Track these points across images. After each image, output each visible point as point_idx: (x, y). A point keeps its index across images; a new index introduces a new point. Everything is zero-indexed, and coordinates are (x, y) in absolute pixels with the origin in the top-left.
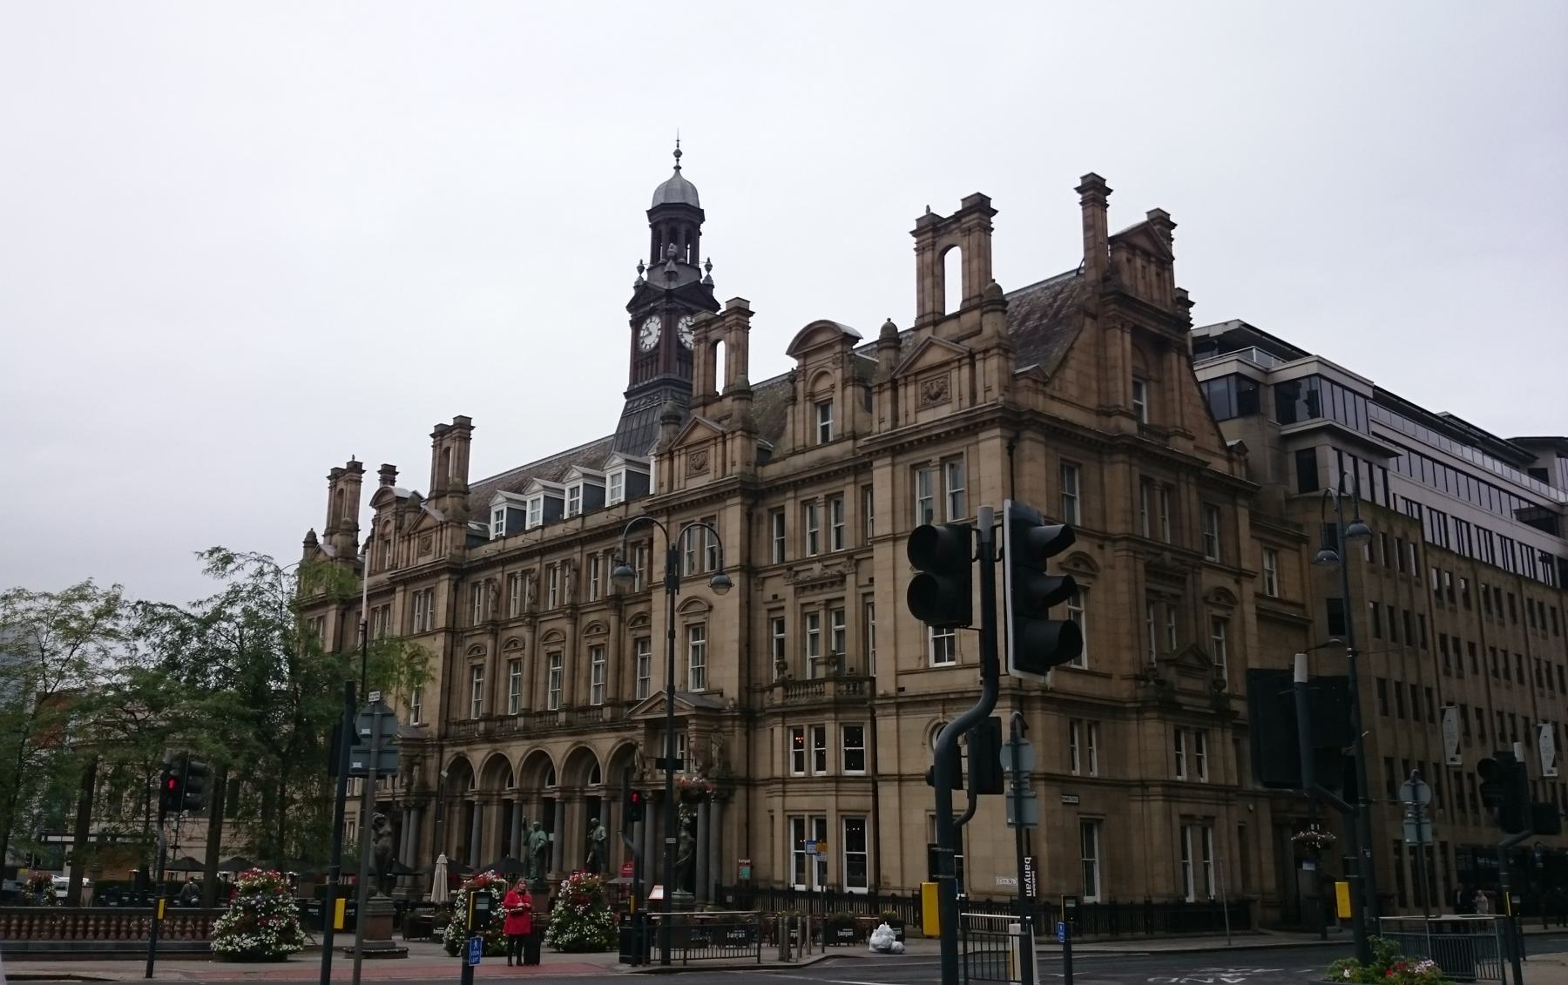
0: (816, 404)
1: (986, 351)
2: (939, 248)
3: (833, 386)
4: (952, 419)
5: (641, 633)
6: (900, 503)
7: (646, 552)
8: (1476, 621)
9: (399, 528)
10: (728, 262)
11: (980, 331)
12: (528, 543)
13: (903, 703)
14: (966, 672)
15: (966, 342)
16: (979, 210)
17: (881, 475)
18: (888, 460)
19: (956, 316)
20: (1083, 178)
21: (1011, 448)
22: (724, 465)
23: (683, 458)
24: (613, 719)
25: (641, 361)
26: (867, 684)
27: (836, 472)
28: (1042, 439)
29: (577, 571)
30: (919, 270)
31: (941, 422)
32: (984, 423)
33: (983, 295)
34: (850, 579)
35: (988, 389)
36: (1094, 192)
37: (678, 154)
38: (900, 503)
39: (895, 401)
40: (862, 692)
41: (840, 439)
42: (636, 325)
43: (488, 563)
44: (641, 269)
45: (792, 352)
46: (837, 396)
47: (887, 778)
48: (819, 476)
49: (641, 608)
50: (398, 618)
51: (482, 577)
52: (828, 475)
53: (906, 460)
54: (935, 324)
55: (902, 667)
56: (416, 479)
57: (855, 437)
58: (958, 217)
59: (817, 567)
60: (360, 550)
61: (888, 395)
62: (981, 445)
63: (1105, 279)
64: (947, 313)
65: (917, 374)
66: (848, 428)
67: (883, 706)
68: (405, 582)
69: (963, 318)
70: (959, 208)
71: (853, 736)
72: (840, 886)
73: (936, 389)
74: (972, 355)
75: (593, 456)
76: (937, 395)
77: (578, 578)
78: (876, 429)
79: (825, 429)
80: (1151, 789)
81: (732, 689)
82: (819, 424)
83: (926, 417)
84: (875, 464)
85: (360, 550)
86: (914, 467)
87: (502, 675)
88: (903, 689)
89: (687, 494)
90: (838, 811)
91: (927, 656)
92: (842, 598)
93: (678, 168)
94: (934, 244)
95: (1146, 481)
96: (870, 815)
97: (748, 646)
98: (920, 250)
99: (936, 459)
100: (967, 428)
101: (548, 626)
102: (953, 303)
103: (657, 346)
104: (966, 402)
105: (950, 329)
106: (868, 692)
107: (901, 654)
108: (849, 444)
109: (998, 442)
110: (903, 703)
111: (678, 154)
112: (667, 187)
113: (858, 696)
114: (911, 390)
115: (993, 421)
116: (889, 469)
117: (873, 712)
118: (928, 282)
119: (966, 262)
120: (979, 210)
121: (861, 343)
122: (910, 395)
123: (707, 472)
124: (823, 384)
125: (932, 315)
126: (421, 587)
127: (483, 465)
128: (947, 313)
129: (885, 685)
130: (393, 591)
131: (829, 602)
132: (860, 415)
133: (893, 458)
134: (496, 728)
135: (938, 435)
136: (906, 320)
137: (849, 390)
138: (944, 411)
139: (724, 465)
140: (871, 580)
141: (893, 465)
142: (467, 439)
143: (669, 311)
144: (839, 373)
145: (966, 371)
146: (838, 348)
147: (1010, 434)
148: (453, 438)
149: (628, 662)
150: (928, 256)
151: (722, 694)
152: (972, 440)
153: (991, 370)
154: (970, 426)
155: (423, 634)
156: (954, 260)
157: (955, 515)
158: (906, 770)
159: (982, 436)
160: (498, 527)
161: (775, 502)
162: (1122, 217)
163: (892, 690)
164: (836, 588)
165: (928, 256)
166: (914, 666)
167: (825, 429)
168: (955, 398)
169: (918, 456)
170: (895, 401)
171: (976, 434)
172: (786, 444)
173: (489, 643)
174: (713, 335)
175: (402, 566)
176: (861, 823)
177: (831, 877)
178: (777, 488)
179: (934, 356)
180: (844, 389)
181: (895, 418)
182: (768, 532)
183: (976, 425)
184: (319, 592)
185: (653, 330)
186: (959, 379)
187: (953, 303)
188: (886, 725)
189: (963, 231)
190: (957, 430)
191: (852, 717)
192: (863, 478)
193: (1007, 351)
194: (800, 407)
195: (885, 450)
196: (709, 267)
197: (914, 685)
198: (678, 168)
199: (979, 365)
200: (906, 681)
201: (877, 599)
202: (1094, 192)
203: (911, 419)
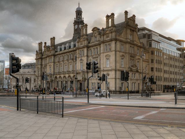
9: (47, 50)
10: (86, 18)
24: (68, 73)
34: (99, 57)
37: (79, 4)
39: (103, 37)
42: (74, 26)
43: (58, 55)
44: (75, 19)
45: (92, 30)
51: (57, 56)
54: (108, 28)
56: (49, 44)
57: (99, 41)
59: (95, 56)
63: (127, 23)
75: (69, 42)
83: (107, 39)
89: (106, 40)
93: (79, 6)
101: (65, 62)
111: (79, 4)
112: (77, 9)
114: (105, 36)
124: (96, 35)
127: (57, 42)
134: (59, 73)
138: (109, 39)
142: (54, 40)
143: (78, 24)
148: (53, 39)
155: (51, 63)
161: (90, 48)
163: (103, 70)
170: (103, 37)
172: (91, 41)
173: (67, 62)
174: (83, 28)
181: (103, 39)
182: (89, 52)
185: (76, 26)
186: (110, 35)
194: (93, 37)
196: (83, 18)
197: (105, 69)
198: (79, 6)
200: (104, 69)
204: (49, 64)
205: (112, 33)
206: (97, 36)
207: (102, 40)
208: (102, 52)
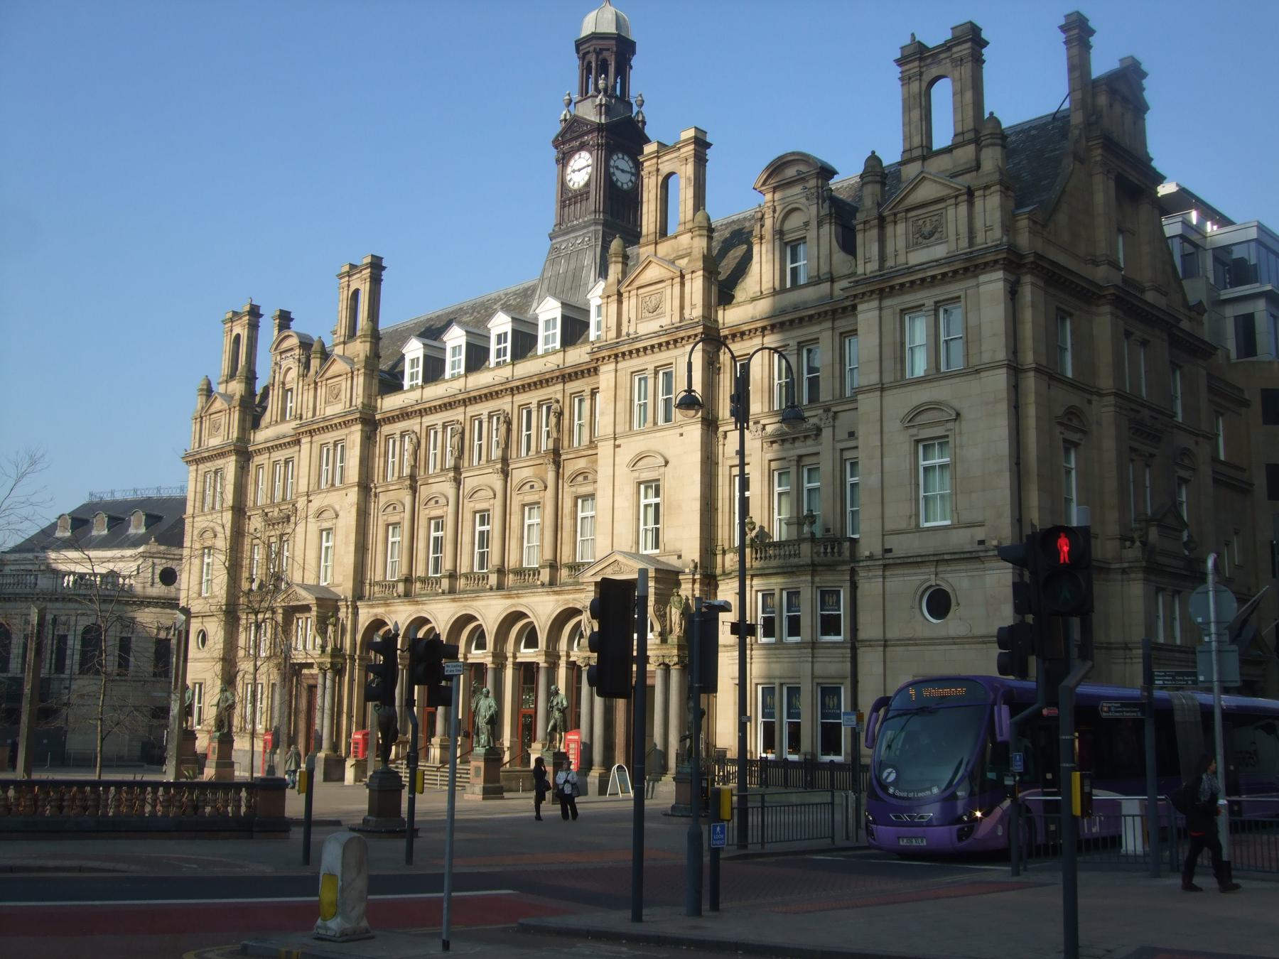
0: (786, 244)
1: (986, 187)
2: (927, 78)
3: (807, 224)
4: (949, 260)
5: (584, 490)
6: (887, 351)
7: (586, 404)
8: (513, 544)
11: (978, 167)
12: (451, 392)
13: (889, 562)
14: (961, 531)
15: (960, 179)
16: (971, 41)
17: (867, 315)
18: (875, 304)
19: (947, 151)
20: (1067, 16)
21: (1013, 293)
22: (682, 308)
23: (633, 300)
25: (569, 198)
26: (847, 545)
27: (811, 317)
28: (1042, 284)
29: (509, 423)
30: (904, 100)
31: (937, 262)
32: (986, 264)
33: (979, 130)
34: (827, 433)
35: (988, 229)
36: (1078, 32)
38: (887, 351)
39: (882, 241)
40: (840, 554)
41: (815, 281)
46: (811, 234)
47: (869, 643)
48: (792, 322)
49: (581, 464)
50: (304, 470)
52: (801, 319)
53: (894, 303)
54: (924, 158)
55: (889, 526)
58: (947, 47)
60: (258, 399)
61: (874, 233)
62: (982, 288)
64: (935, 148)
65: (908, 211)
66: (825, 269)
67: (868, 568)
68: (311, 433)
69: (955, 152)
70: (949, 36)
71: (827, 596)
72: (814, 755)
73: (928, 228)
74: (970, 193)
76: (931, 234)
77: (509, 430)
78: (860, 270)
79: (795, 272)
80: (1134, 652)
81: (691, 551)
82: (789, 266)
83: (917, 257)
84: (860, 308)
85: (258, 399)
86: (903, 312)
87: (422, 534)
88: (890, 551)
89: (910, 270)
90: (813, 677)
91: (917, 515)
92: (818, 454)
94: (921, 74)
95: (1128, 334)
96: (848, 681)
97: (1018, 464)
98: (905, 80)
99: (930, 303)
100: (966, 270)
102: (942, 136)
103: (587, 184)
104: (964, 243)
105: (945, 162)
106: (847, 553)
107: (889, 512)
108: (825, 287)
109: (1001, 285)
110: (889, 562)
113: (836, 557)
114: (901, 228)
115: (996, 262)
116: (876, 313)
117: (853, 572)
118: (916, 114)
119: (958, 93)
120: (971, 41)
121: (836, 178)
122: (899, 234)
123: (662, 315)
125: (921, 151)
126: (330, 437)
128: (935, 148)
129: (869, 545)
130: (298, 442)
131: (800, 457)
132: (839, 256)
133: (881, 300)
135: (934, 277)
136: (891, 156)
137: (826, 229)
138: (939, 251)
139: (682, 308)
140: (852, 435)
141: (881, 309)
144: (814, 210)
145: (963, 209)
146: (812, 183)
147: (1012, 278)
149: (567, 522)
150: (915, 86)
151: (680, 557)
152: (972, 282)
153: (990, 208)
154: (970, 266)
156: (943, 95)
157: (948, 365)
158: (892, 634)
159: (982, 278)
160: (412, 377)
162: (1102, 63)
163: (878, 550)
164: (810, 442)
165: (915, 86)
166: (903, 525)
167: (795, 272)
168: (952, 237)
169: (909, 299)
170: (882, 241)
171: (976, 276)
175: (308, 415)
176: (837, 691)
177: (806, 744)
178: (743, 334)
179: (927, 192)
180: (820, 224)
181: (882, 258)
183: (976, 266)
184: (215, 442)
186: (956, 216)
187: (942, 136)
188: (870, 586)
189: (953, 61)
190: (955, 272)
191: (827, 580)
192: (843, 324)
193: (1007, 188)
195: (872, 292)
197: (903, 546)
199: (978, 203)
200: (892, 542)
201: (862, 455)
202: (1078, 32)
203: (901, 259)
204: (631, 447)
205: (971, 203)
206: (811, 234)
207: (873, 266)
208: (604, 425)
